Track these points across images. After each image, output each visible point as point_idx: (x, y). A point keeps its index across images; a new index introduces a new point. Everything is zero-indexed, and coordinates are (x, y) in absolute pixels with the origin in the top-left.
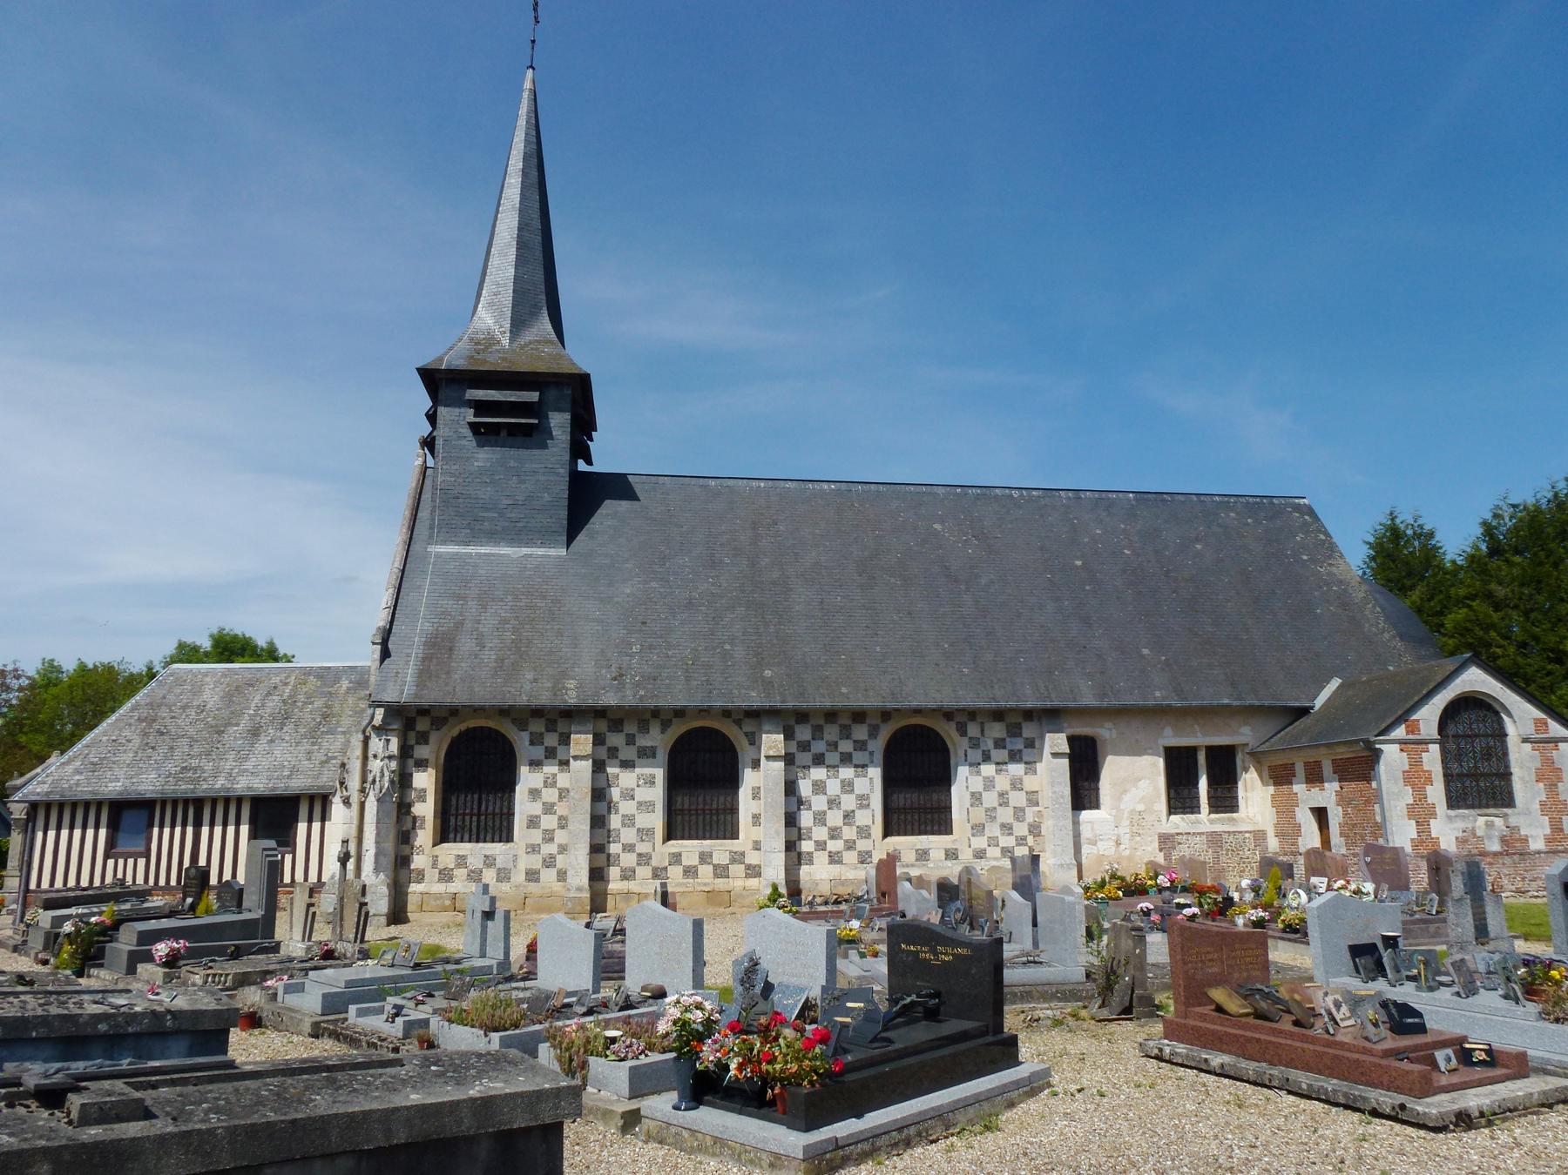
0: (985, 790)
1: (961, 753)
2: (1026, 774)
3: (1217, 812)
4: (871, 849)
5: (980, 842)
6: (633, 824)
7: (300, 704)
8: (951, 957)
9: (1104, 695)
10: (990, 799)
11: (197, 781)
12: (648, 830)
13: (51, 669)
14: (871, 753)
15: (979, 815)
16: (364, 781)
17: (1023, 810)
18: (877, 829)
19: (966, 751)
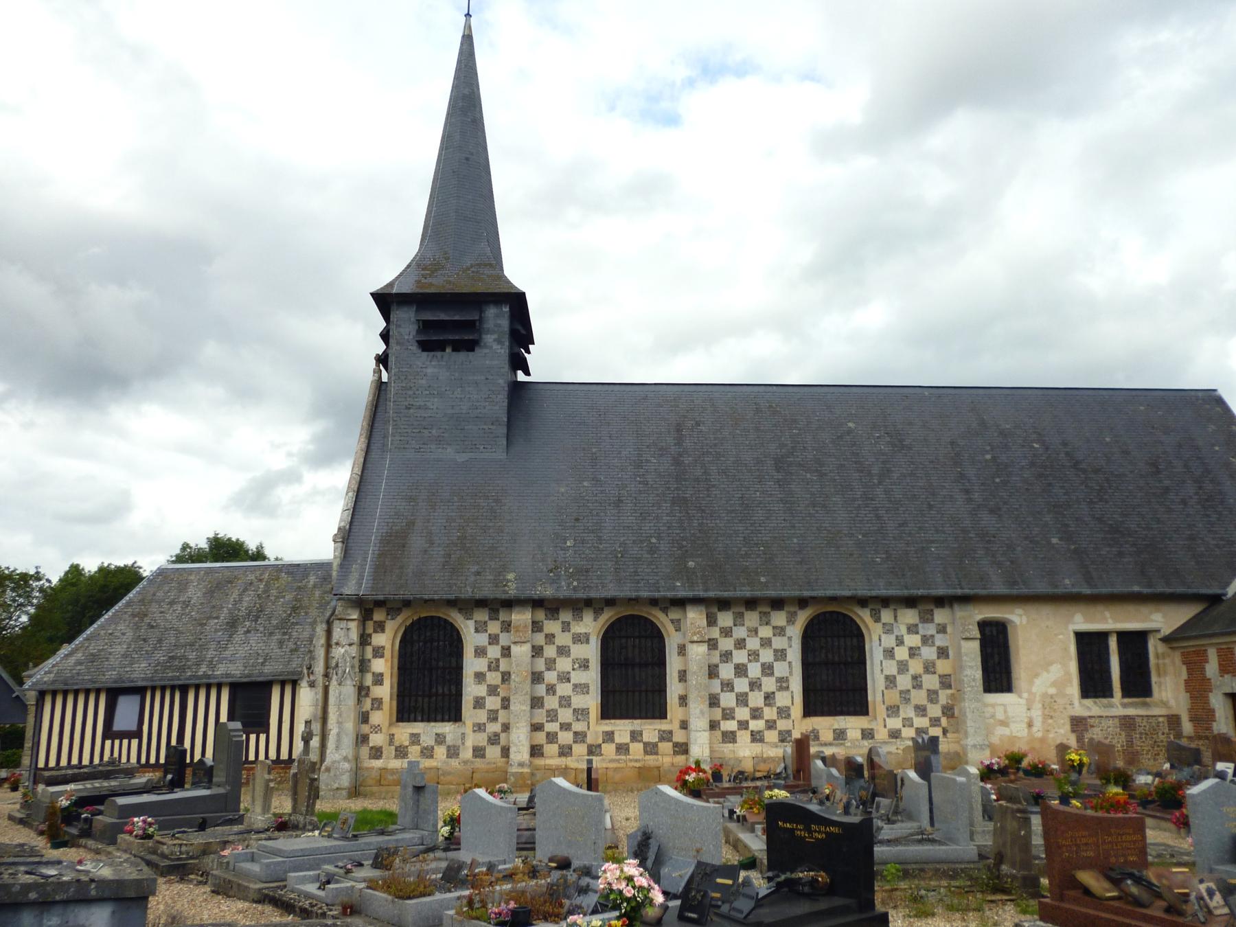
0: (899, 673)
1: (875, 638)
2: (938, 658)
4: (791, 728)
5: (895, 723)
6: (569, 705)
7: (273, 598)
8: (824, 835)
9: (1013, 583)
10: (904, 682)
11: (182, 669)
12: (583, 710)
13: (75, 571)
14: (790, 639)
15: (893, 697)
16: (327, 667)
17: (936, 692)
18: (797, 710)
19: (880, 636)
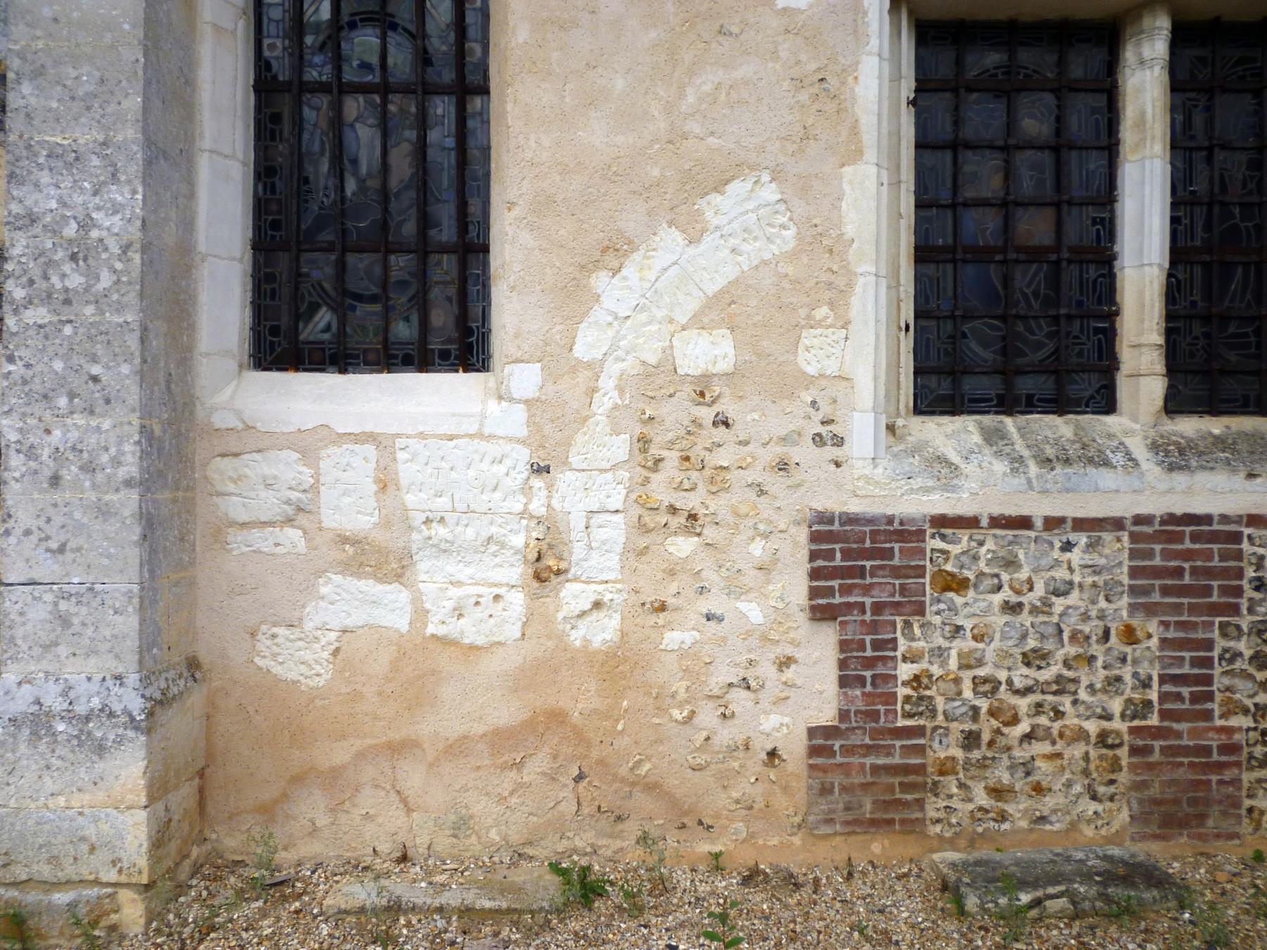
3: (1213, 408)
